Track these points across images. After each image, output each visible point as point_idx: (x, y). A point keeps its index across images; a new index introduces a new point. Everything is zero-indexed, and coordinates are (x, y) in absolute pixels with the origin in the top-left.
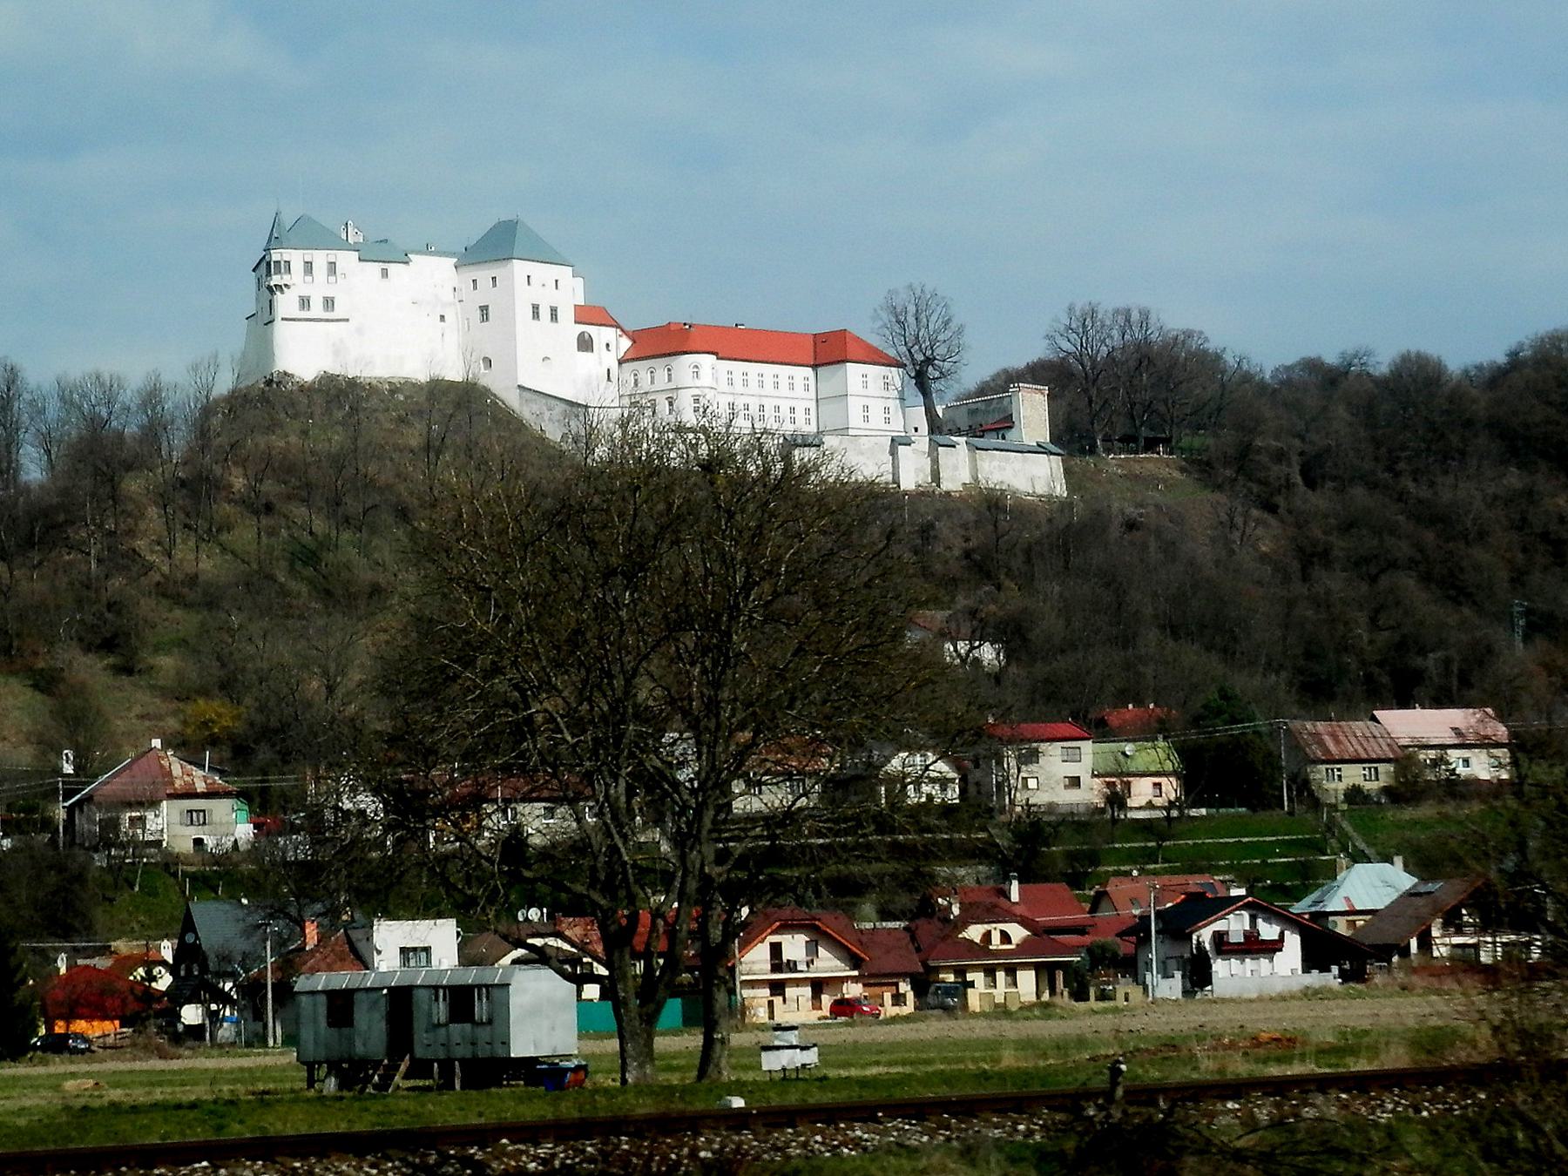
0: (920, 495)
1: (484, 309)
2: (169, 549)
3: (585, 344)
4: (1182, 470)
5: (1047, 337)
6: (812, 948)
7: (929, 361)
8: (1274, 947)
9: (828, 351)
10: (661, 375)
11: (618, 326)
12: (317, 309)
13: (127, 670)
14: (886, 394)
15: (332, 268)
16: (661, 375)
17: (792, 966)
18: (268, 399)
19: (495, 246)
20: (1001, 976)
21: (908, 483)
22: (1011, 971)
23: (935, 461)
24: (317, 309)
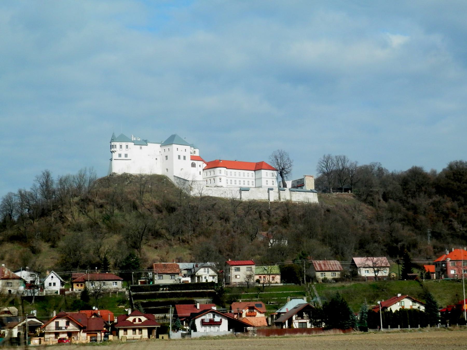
0: (275, 203)
1: (167, 157)
2: (75, 216)
3: (193, 165)
4: (354, 197)
5: (319, 163)
6: (68, 324)
7: (283, 169)
8: (219, 324)
9: (258, 167)
10: (212, 173)
11: (202, 161)
12: (123, 157)
13: (53, 246)
14: (273, 177)
15: (127, 146)
16: (212, 173)
17: (61, 328)
18: (112, 179)
19: (170, 141)
20: (137, 331)
21: (272, 200)
22: (140, 330)
23: (279, 194)
24: (123, 157)
